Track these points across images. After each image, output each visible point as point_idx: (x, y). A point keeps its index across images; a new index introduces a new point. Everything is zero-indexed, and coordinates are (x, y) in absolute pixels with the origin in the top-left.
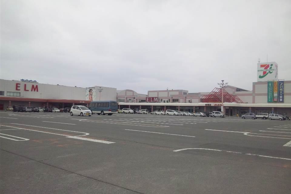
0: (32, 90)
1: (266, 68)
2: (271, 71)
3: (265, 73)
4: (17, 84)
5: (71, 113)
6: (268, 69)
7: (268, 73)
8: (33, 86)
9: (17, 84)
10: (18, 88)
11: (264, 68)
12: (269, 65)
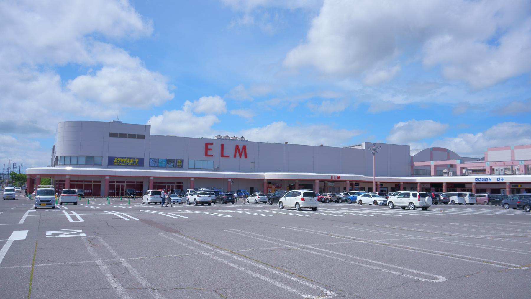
0: (235, 156)
4: (207, 144)
5: (281, 204)
8: (237, 147)
9: (207, 144)
10: (209, 153)
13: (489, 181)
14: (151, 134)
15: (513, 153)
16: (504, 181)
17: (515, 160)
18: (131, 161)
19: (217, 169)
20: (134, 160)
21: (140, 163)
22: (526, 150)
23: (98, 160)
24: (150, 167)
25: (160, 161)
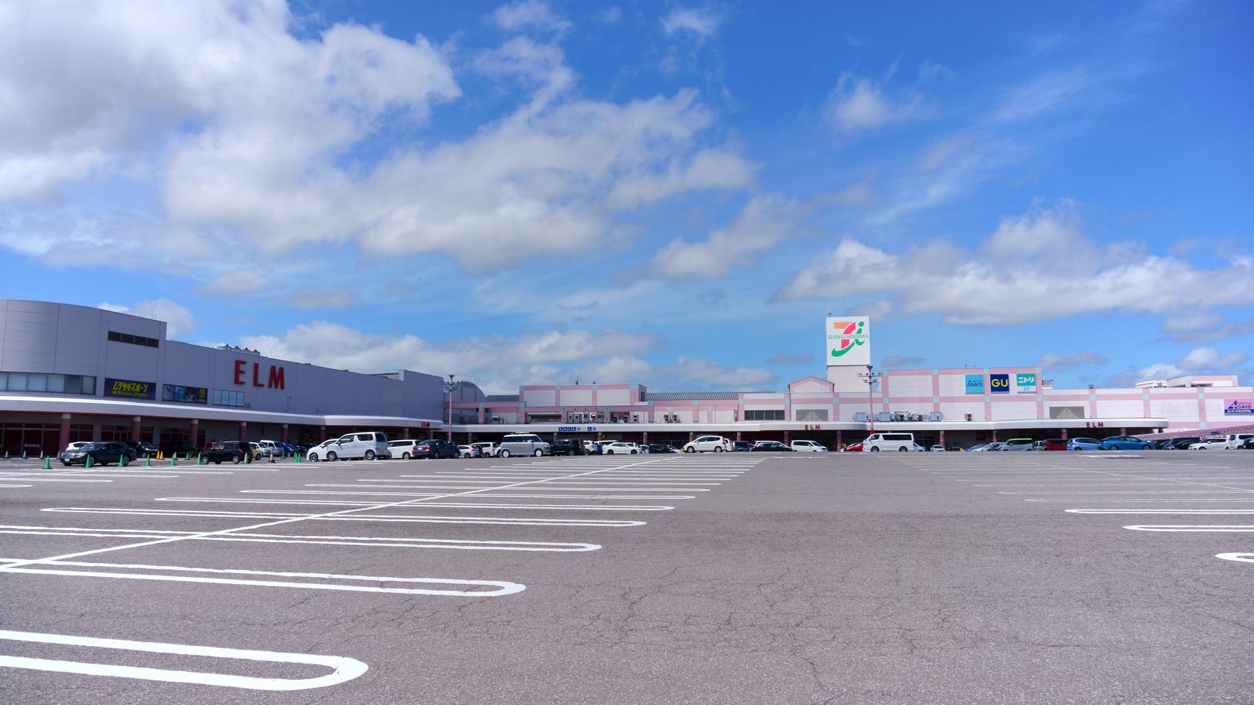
1: (849, 331)
2: (860, 341)
3: (845, 343)
6: (854, 332)
7: (853, 344)
8: (273, 368)
11: (843, 330)
12: (854, 324)
13: (577, 431)
14: (167, 339)
15: (595, 394)
16: (467, 431)
17: (792, 405)
18: (138, 388)
19: (248, 407)
20: (142, 386)
21: (148, 392)
22: (765, 394)
23: (88, 384)
24: (164, 401)
25: (177, 390)
